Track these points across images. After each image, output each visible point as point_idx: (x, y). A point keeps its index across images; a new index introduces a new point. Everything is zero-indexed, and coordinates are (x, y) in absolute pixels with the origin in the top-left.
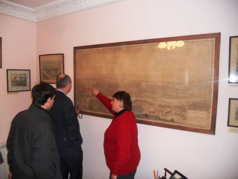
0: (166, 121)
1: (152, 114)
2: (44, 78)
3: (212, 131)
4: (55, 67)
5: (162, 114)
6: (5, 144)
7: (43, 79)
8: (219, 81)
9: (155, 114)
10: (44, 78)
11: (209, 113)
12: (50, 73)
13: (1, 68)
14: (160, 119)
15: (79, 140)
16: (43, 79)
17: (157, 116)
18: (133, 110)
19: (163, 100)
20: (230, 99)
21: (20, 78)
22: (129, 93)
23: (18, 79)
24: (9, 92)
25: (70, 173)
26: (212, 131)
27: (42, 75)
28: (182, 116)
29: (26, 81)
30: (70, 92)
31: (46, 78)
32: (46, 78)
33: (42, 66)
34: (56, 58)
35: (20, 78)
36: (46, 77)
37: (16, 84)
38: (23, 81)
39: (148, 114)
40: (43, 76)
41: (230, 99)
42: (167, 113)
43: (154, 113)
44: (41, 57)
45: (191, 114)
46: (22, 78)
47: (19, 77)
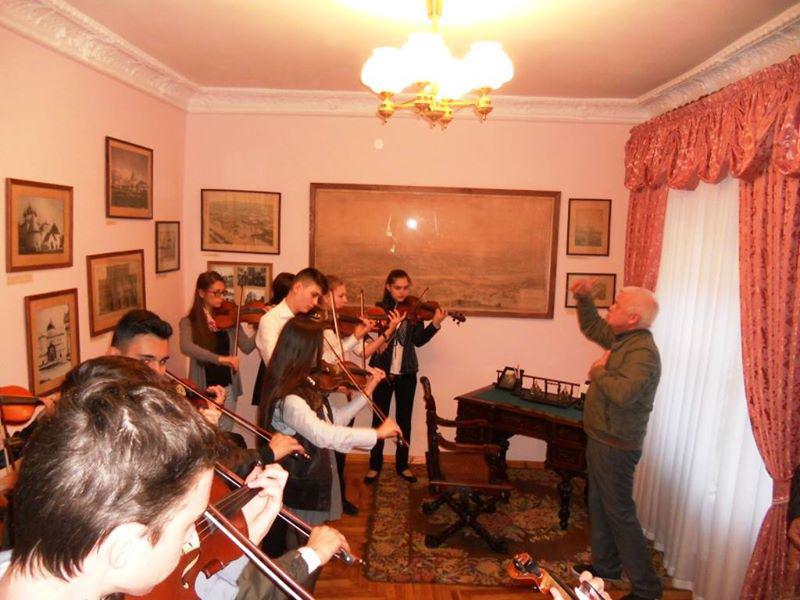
0: (490, 307)
1: (468, 299)
3: (550, 315)
5: (484, 299)
6: (371, 448)
7: (210, 242)
9: (474, 299)
11: (545, 291)
14: (480, 305)
15: (644, 432)
17: (476, 302)
19: (486, 276)
22: (399, 268)
24: (161, 272)
25: (137, 389)
26: (550, 315)
28: (513, 298)
30: (583, 328)
31: (219, 240)
32: (219, 240)
36: (221, 238)
39: (462, 299)
40: (211, 236)
41: (568, 274)
42: (491, 296)
43: (471, 297)
45: (523, 294)
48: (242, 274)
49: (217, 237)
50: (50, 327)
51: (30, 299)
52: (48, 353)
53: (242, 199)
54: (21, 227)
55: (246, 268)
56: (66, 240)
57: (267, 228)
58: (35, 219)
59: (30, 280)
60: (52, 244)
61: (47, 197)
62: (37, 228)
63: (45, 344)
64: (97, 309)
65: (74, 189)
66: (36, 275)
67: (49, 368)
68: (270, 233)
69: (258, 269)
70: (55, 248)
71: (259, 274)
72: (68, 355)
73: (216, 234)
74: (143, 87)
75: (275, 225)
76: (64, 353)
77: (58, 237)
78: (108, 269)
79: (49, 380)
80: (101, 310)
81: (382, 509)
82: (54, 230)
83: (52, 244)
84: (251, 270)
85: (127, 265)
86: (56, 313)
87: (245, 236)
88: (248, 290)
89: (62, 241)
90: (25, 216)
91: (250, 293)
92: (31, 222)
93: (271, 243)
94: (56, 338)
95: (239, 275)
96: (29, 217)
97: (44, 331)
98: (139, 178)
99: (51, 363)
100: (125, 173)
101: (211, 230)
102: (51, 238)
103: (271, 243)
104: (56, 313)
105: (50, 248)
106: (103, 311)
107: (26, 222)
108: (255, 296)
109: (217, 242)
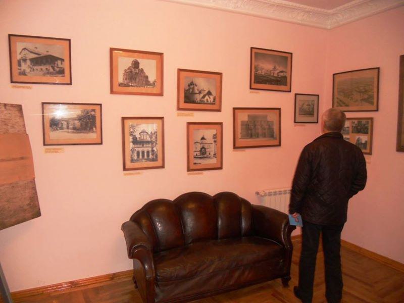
2: (339, 104)
4: (361, 88)
8: (25, 123)
10: (339, 104)
12: (352, 98)
13: (402, 57)
16: (337, 106)
18: (342, 268)
20: (101, 105)
21: (307, 105)
23: (305, 107)
27: (336, 100)
29: (313, 111)
31: (342, 104)
32: (342, 104)
33: (338, 89)
34: (369, 74)
35: (307, 105)
36: (344, 103)
37: (303, 113)
38: (311, 110)
40: (337, 102)
44: (297, 96)
46: (309, 105)
47: (306, 104)
48: (354, 125)
49: (341, 103)
50: (203, 138)
51: (189, 124)
52: (201, 151)
53: (355, 76)
54: (186, 91)
55: (356, 122)
56: (217, 99)
57: (370, 93)
58: (196, 88)
59: (192, 115)
60: (207, 100)
61: (201, 77)
62: (196, 91)
63: (199, 147)
64: (239, 135)
65: (223, 74)
66: (196, 114)
67: (200, 158)
68: (371, 97)
69: (364, 122)
70: (209, 102)
71: (365, 125)
72: (215, 154)
73: (341, 101)
74: (294, 20)
75: (375, 89)
76: (212, 153)
77: (211, 97)
78: (272, 122)
79: (200, 164)
80: (242, 136)
81: (215, 162)
82: (209, 93)
83: (207, 100)
84: (359, 122)
85: (267, 115)
86: (209, 133)
87: (357, 101)
88: (357, 136)
89: (214, 99)
90: (189, 86)
91: (359, 138)
92: (193, 89)
93: (372, 103)
94: (207, 145)
95: (352, 127)
96: (192, 86)
97: (199, 140)
98: (280, 69)
99: (201, 156)
100: (267, 67)
101: (338, 98)
102: (207, 97)
103: (372, 103)
104: (209, 133)
105: (206, 102)
106: (243, 137)
107: (189, 89)
108: (361, 140)
109: (341, 106)
